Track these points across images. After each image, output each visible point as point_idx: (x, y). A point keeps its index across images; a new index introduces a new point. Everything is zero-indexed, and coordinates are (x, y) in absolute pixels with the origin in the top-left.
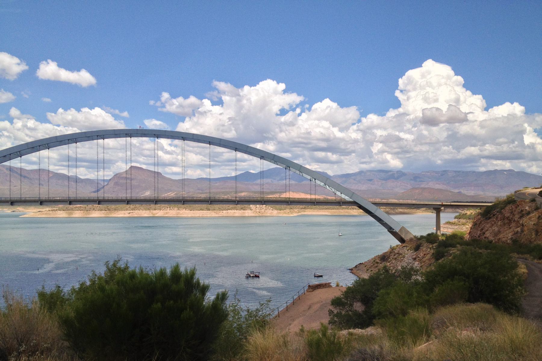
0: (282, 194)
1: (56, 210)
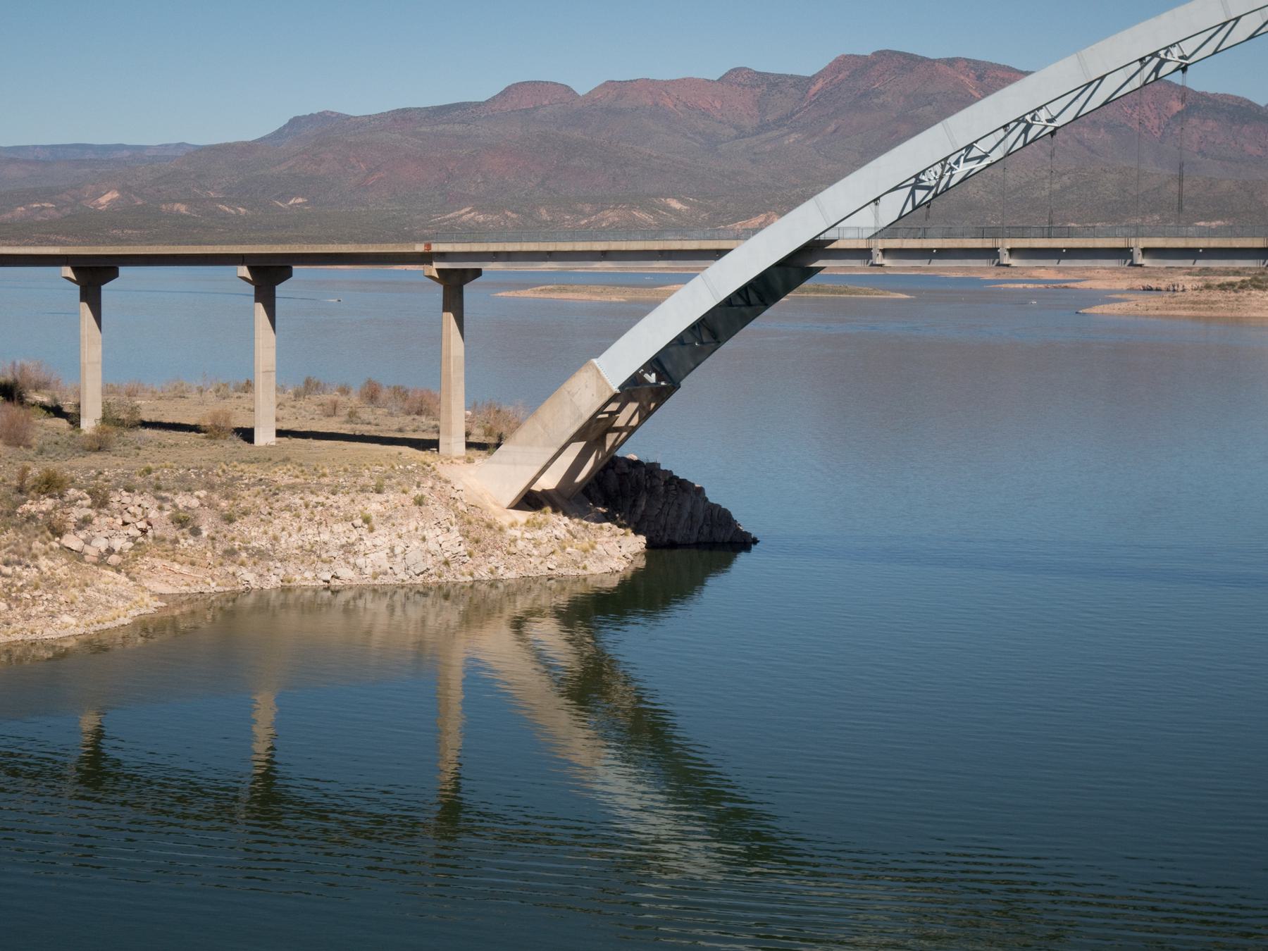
1: (1243, 286)
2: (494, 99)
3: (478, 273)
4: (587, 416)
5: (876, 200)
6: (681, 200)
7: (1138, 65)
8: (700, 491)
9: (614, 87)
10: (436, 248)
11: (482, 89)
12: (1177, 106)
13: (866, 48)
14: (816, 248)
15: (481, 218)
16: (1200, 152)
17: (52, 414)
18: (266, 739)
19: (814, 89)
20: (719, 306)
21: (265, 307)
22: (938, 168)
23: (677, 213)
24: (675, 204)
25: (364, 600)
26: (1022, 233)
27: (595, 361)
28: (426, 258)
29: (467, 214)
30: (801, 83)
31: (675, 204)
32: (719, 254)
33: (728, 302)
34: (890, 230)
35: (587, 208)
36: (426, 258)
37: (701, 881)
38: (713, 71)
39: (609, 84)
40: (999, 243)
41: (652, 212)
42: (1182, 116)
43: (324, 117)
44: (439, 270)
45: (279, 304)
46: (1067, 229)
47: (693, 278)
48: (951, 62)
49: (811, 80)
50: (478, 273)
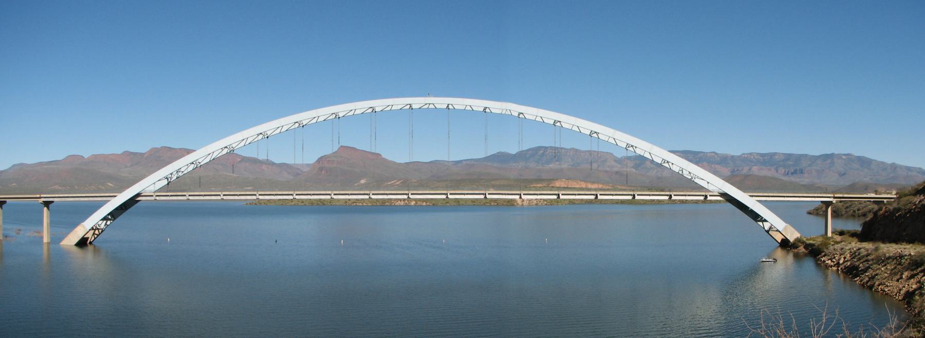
0: (552, 183)
4: (81, 237)
5: (154, 183)
6: (112, 184)
7: (221, 150)
9: (95, 156)
10: (42, 196)
11: (60, 157)
13: (158, 146)
14: (138, 195)
15: (60, 188)
17: (919, 261)
20: (114, 210)
21: (50, 204)
23: (111, 187)
24: (110, 185)
27: (83, 224)
29: (56, 187)
30: (142, 154)
31: (110, 185)
32: (115, 196)
33: (117, 209)
34: (160, 190)
35: (87, 185)
38: (119, 151)
43: (22, 164)
44: (43, 201)
45: (50, 208)
46: (644, 152)
47: (105, 204)
48: (180, 149)
49: (144, 154)
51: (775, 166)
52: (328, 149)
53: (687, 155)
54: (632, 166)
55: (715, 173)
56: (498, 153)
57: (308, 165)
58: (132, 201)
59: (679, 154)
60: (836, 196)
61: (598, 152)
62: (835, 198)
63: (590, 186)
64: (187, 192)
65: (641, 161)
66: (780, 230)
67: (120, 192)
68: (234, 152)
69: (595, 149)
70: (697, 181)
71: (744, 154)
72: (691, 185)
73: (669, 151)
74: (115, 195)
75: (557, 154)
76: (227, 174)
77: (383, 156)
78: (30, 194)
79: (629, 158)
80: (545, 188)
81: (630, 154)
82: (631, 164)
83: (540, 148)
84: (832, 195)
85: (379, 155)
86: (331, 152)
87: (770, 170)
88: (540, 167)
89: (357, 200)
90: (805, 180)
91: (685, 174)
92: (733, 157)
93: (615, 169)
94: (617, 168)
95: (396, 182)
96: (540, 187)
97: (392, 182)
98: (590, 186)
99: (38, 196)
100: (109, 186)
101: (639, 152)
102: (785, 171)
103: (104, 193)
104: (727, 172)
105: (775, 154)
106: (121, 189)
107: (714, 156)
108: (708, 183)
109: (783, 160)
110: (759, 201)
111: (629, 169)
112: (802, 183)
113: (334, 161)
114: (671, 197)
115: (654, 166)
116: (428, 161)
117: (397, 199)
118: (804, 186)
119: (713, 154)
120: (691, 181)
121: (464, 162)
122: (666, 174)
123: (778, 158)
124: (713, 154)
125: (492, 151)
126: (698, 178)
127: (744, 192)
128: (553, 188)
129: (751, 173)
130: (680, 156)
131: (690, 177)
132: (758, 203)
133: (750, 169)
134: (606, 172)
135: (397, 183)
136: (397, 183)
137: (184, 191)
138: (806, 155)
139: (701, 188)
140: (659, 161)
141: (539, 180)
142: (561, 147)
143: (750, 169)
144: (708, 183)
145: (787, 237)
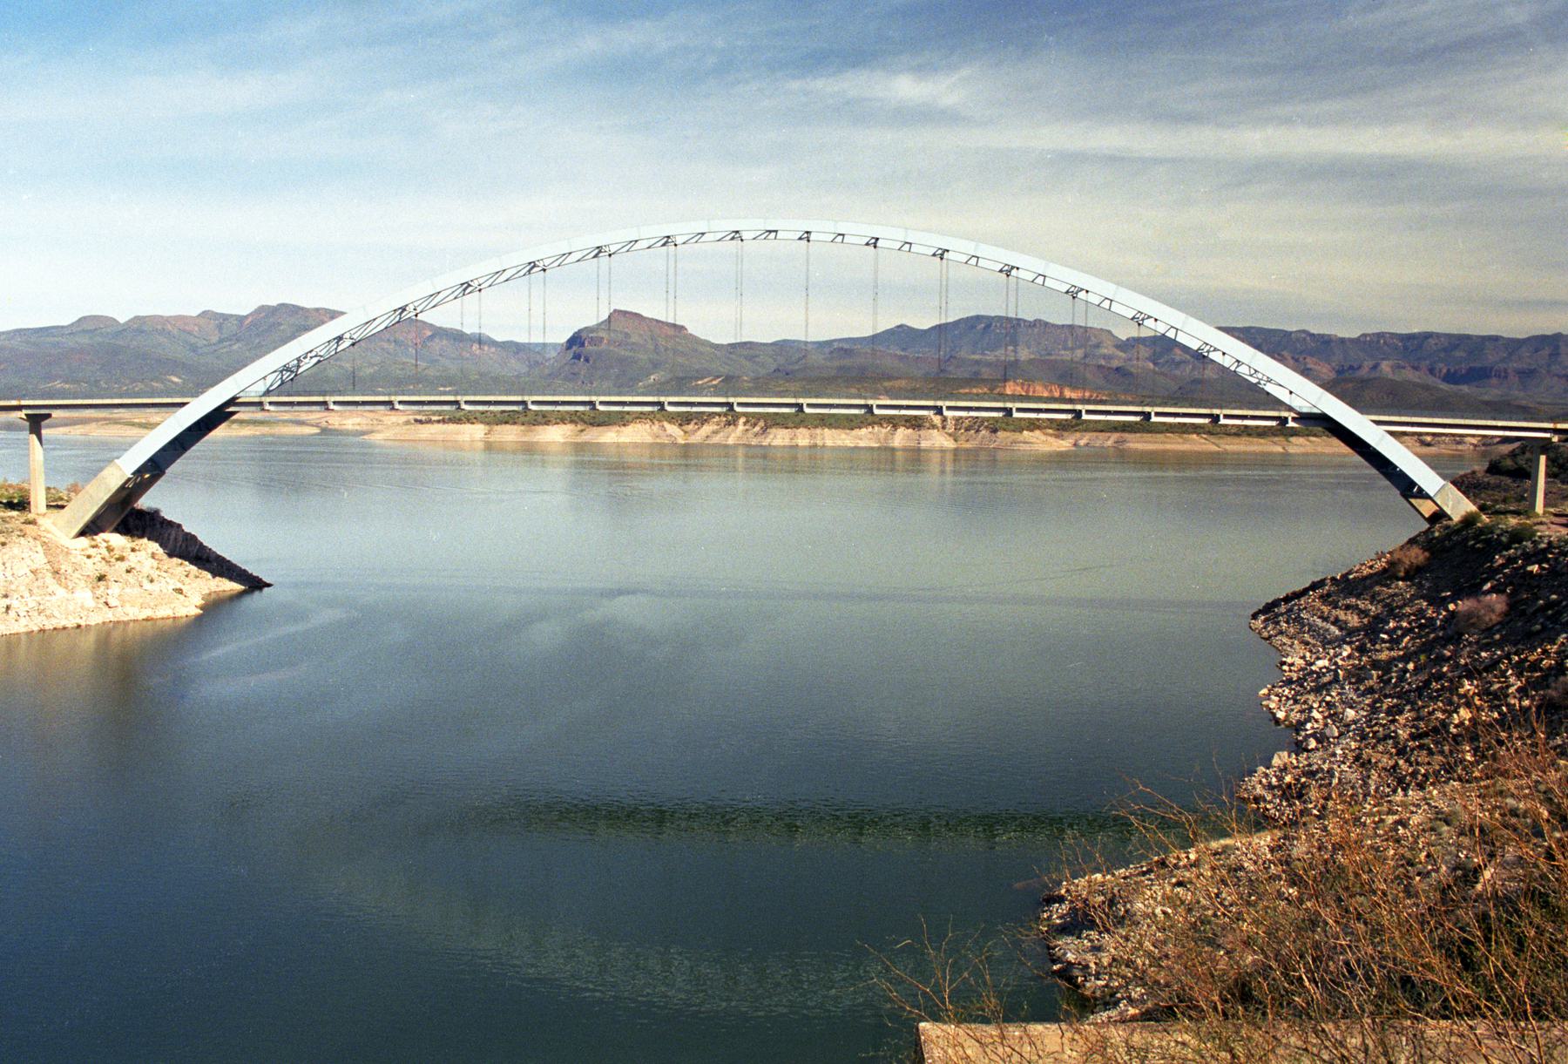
2: (73, 324)
3: (49, 416)
8: (179, 526)
12: (429, 333)
14: (232, 401)
16: (440, 355)
18: (91, 574)
19: (247, 322)
21: (43, 420)
22: (296, 362)
23: (175, 383)
24: (175, 379)
25: (426, 371)
26: (340, 393)
28: (19, 408)
29: (58, 384)
31: (175, 379)
32: (183, 405)
33: (190, 429)
34: (268, 393)
36: (19, 408)
37: (383, 442)
39: (137, 318)
40: (327, 398)
41: (162, 383)
42: (432, 338)
48: (317, 310)
50: (49, 416)
51: (1428, 362)
52: (587, 313)
53: (1250, 336)
54: (1147, 355)
55: (1306, 373)
56: (899, 327)
57: (554, 346)
58: (218, 416)
59: (1237, 334)
60: (1559, 426)
61: (1086, 329)
62: (1556, 431)
63: (1068, 393)
64: (462, 395)
65: (1164, 346)
66: (1432, 494)
67: (196, 394)
68: (419, 317)
69: (1080, 322)
70: (1269, 388)
71: (1364, 335)
72: (1255, 395)
73: (1220, 328)
74: (185, 400)
75: (1010, 329)
76: (1248, 473)
77: (690, 331)
78: (121, 397)
79: (1138, 340)
80: (986, 397)
81: (1144, 333)
82: (1144, 352)
83: (978, 318)
84: (1551, 426)
85: (682, 328)
86: (595, 323)
87: (1416, 368)
88: (977, 357)
89: (642, 413)
90: (1492, 392)
91: (1243, 370)
92: (1343, 341)
93: (1115, 364)
94: (1118, 361)
95: (711, 381)
96: (977, 395)
97: (706, 380)
98: (1068, 393)
99: (14, 403)
100: (172, 382)
101: (1161, 328)
102: (1449, 370)
103: (746, 396)
104: (1326, 371)
105: (1427, 336)
106: (198, 389)
107: (1304, 339)
108: (1291, 393)
109: (1445, 350)
110: (1392, 433)
111: (1142, 363)
112: (1486, 398)
113: (603, 338)
114: (1011, 415)
115: (1188, 357)
116: (770, 342)
117: (713, 413)
118: (1487, 403)
119: (1303, 335)
120: (1255, 388)
121: (836, 345)
122: (1209, 373)
123: (1436, 344)
124: (1303, 335)
125: (886, 323)
126: (1269, 380)
127: (1362, 412)
128: (1002, 397)
129: (1378, 375)
130: (1238, 338)
131: (1254, 381)
132: (1388, 436)
133: (1375, 367)
134: (1100, 367)
135: (714, 383)
136: (714, 383)
137: (324, 393)
138: (1495, 339)
139: (1277, 403)
140: (1194, 345)
141: (975, 380)
142: (1019, 317)
143: (1375, 367)
144: (1291, 393)
145: (1445, 509)
